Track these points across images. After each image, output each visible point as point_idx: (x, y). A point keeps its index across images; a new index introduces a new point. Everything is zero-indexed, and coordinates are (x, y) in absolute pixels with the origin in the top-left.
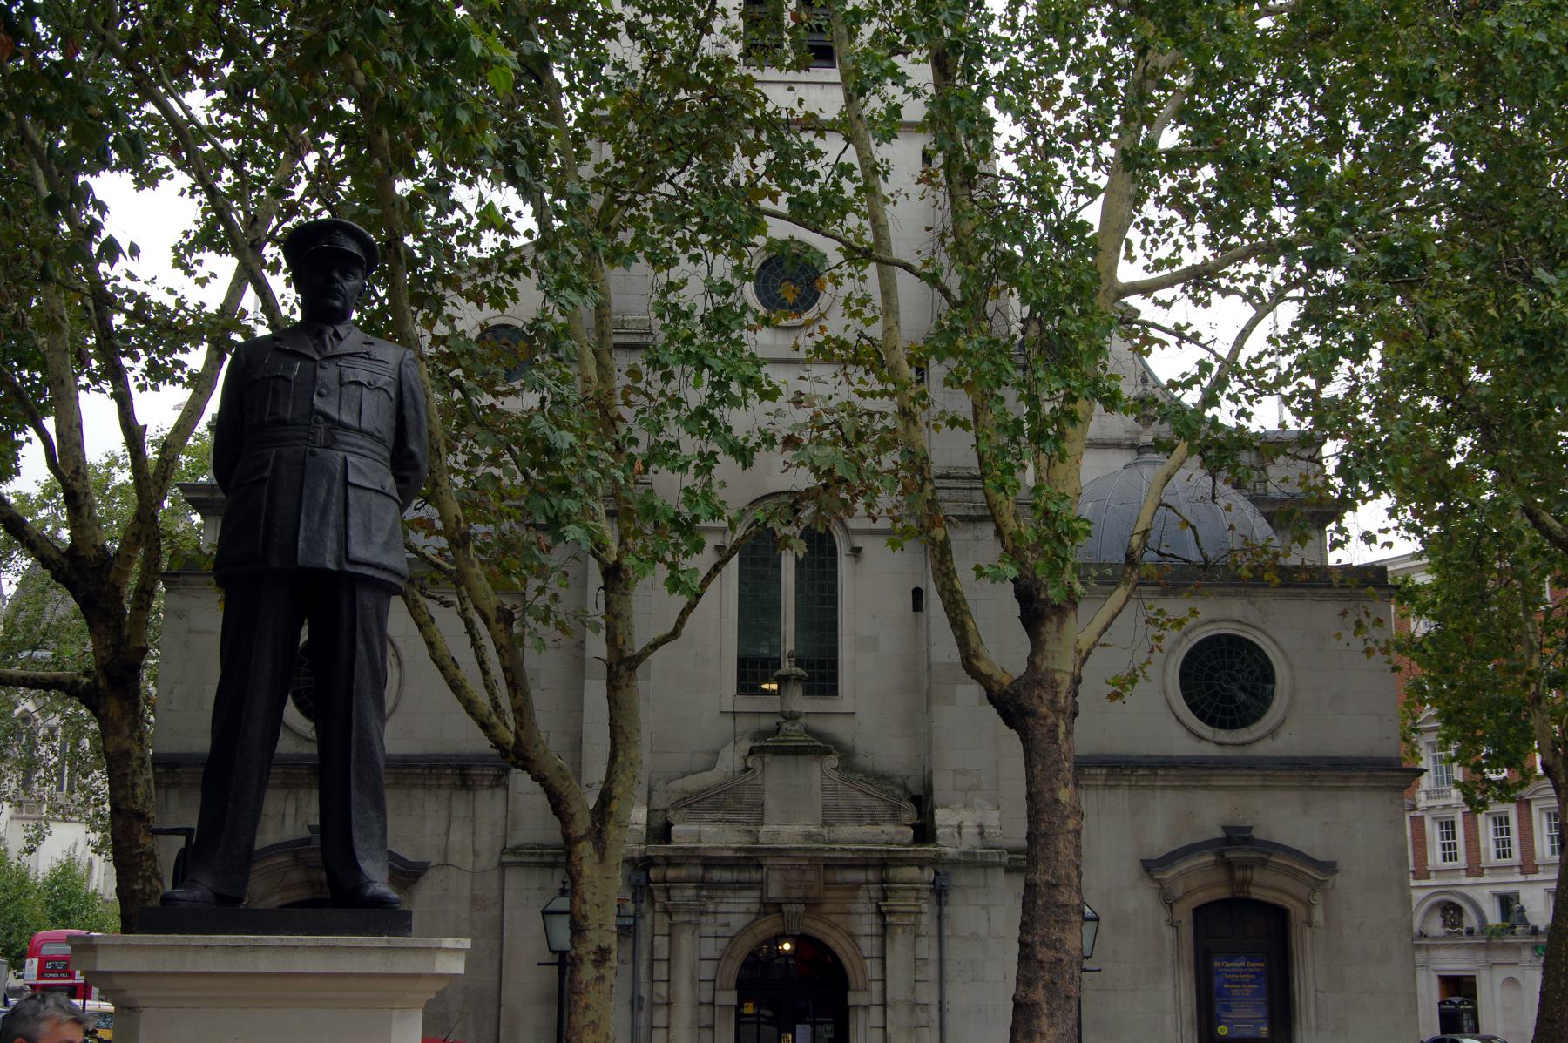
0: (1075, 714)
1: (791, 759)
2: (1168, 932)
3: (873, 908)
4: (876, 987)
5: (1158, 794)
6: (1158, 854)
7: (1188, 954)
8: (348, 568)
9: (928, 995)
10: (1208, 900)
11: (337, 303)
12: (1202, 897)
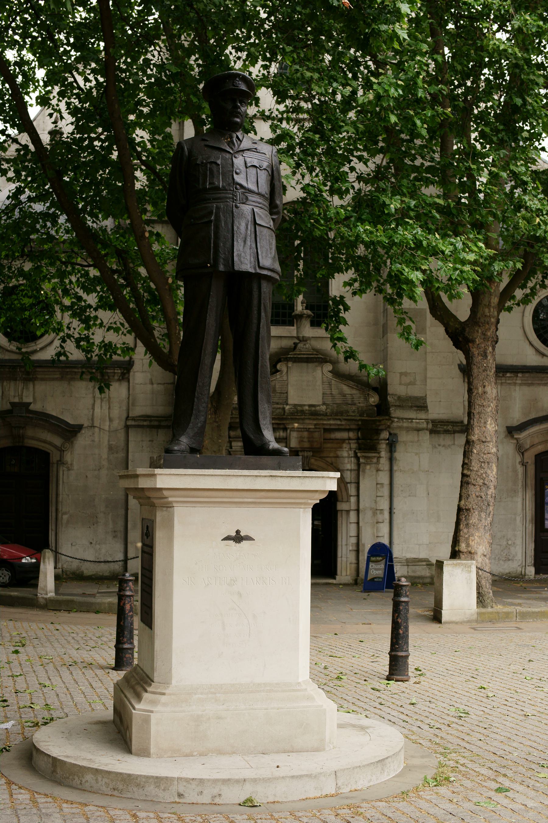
0: (496, 342)
1: (304, 365)
2: (520, 469)
3: (352, 453)
4: (353, 500)
5: (517, 388)
6: (515, 423)
7: (531, 481)
8: (258, 271)
9: (384, 505)
10: (544, 450)
11: (238, 120)
12: (541, 448)
